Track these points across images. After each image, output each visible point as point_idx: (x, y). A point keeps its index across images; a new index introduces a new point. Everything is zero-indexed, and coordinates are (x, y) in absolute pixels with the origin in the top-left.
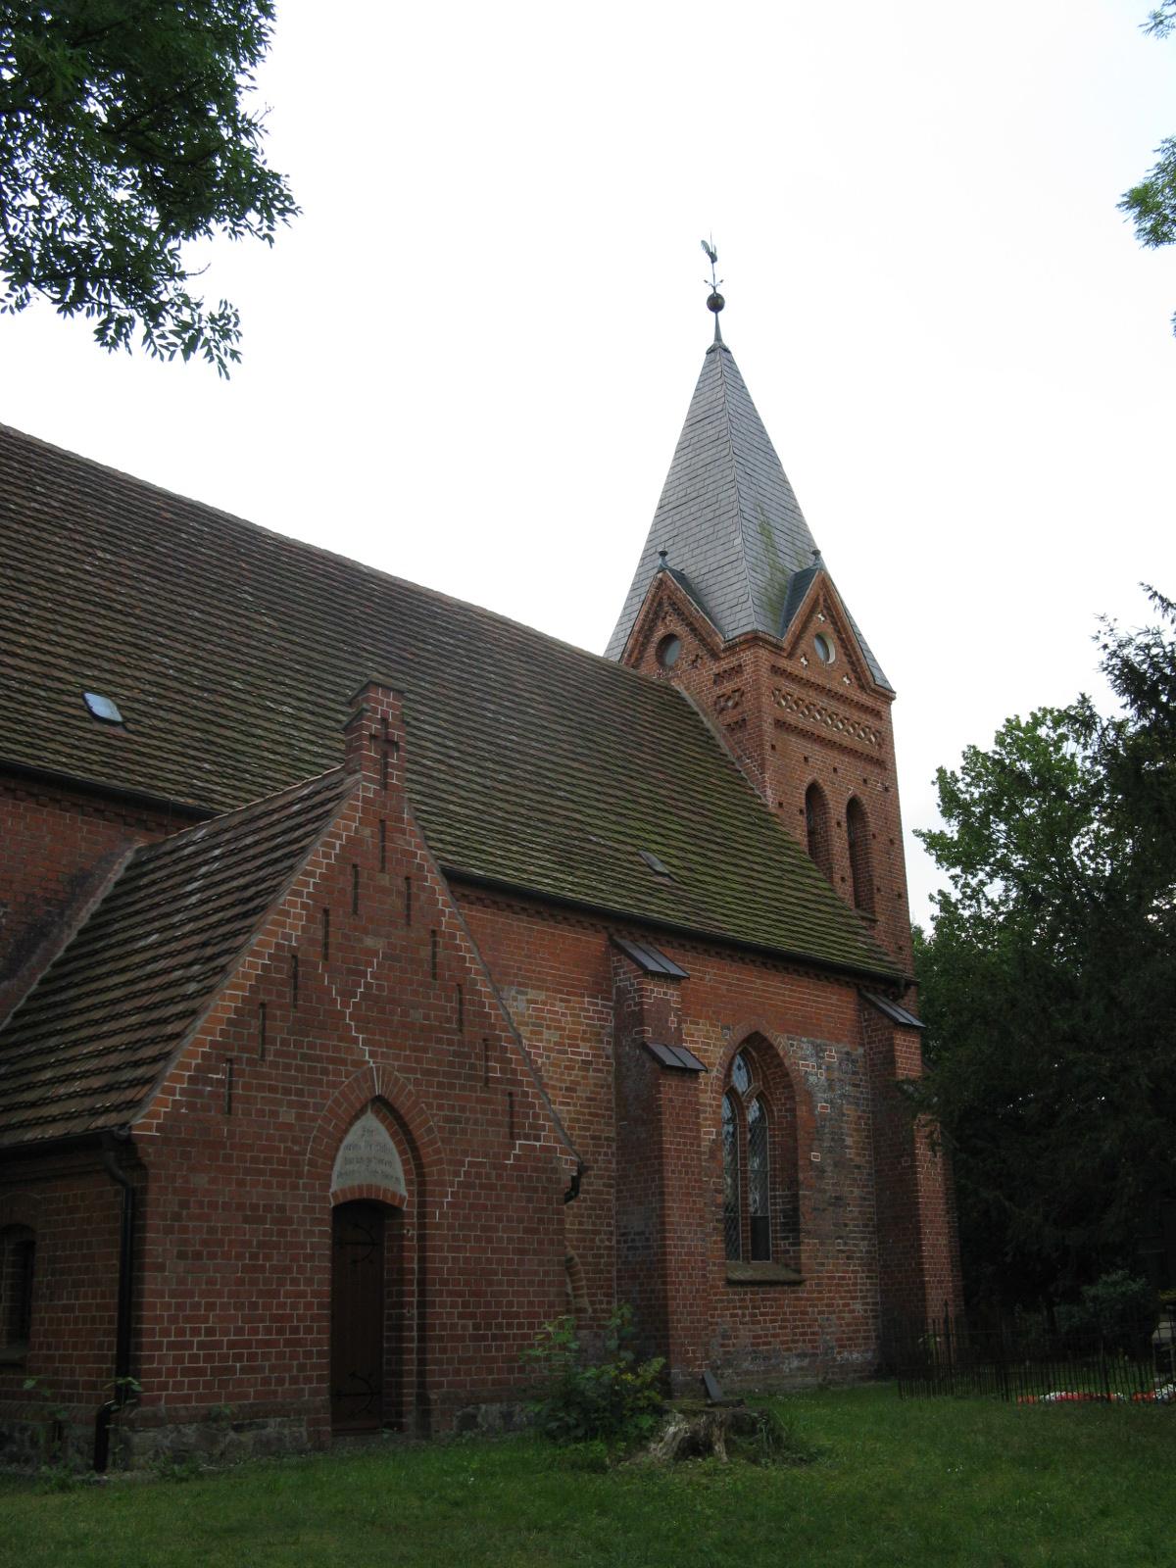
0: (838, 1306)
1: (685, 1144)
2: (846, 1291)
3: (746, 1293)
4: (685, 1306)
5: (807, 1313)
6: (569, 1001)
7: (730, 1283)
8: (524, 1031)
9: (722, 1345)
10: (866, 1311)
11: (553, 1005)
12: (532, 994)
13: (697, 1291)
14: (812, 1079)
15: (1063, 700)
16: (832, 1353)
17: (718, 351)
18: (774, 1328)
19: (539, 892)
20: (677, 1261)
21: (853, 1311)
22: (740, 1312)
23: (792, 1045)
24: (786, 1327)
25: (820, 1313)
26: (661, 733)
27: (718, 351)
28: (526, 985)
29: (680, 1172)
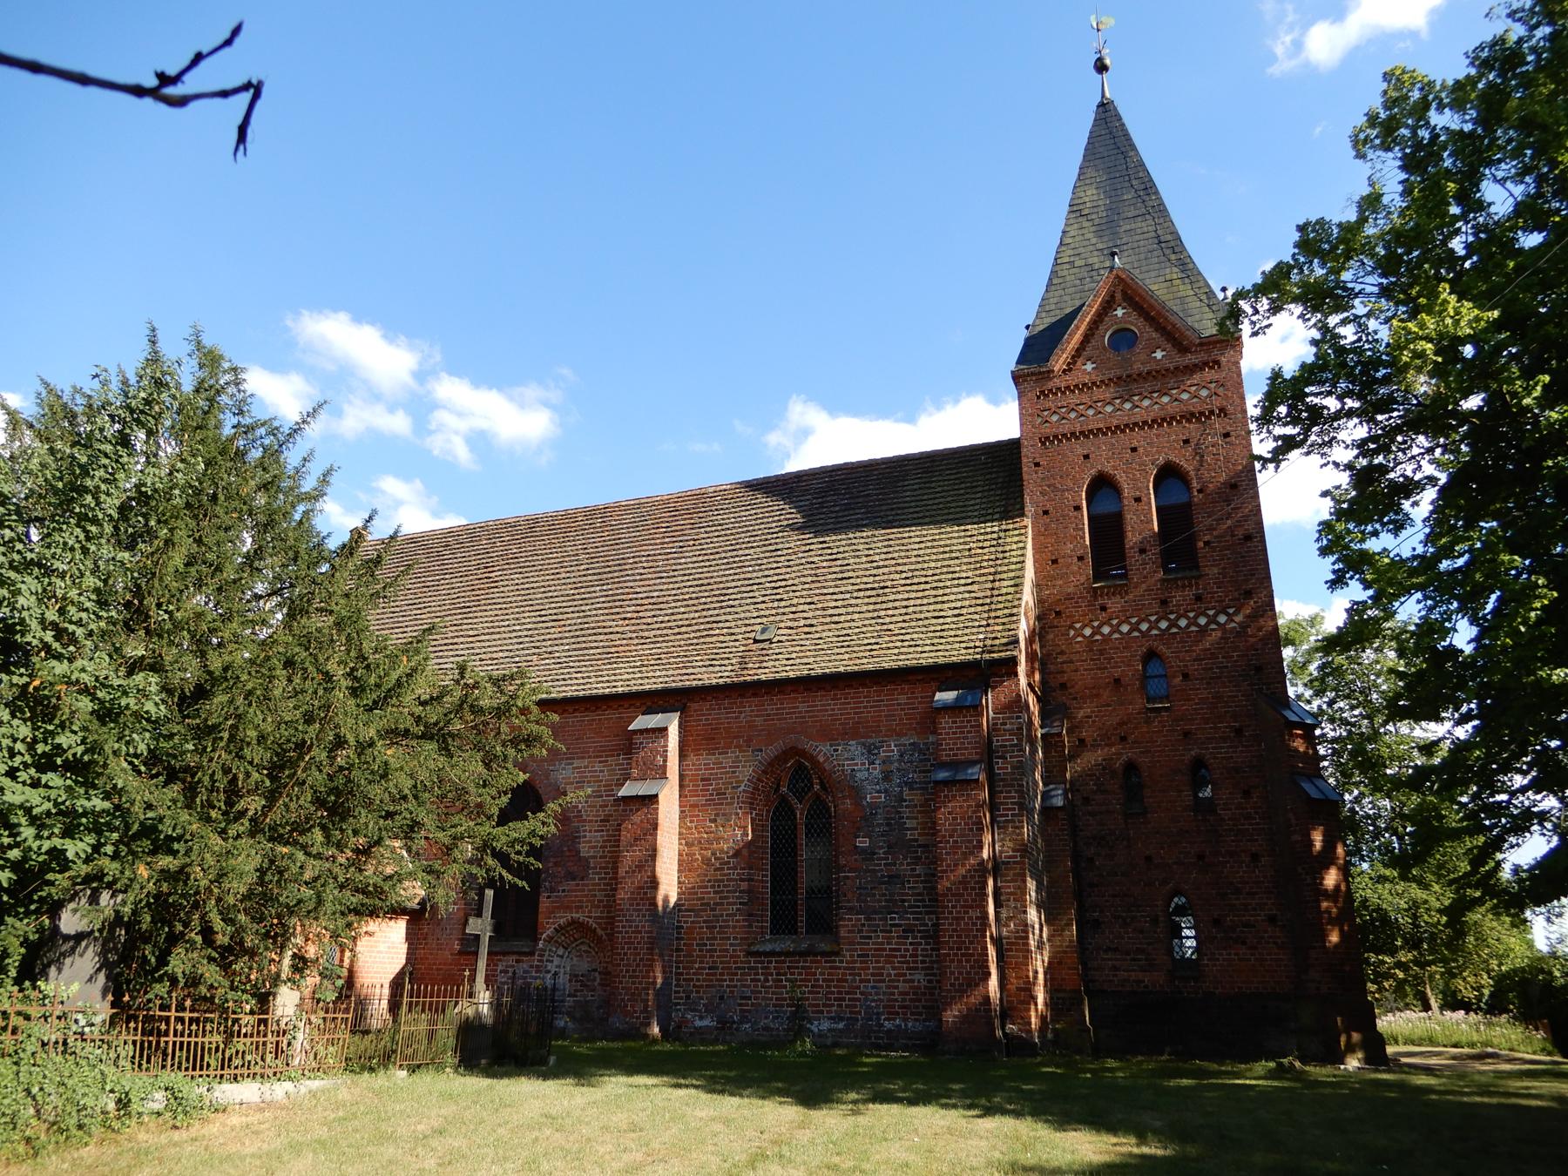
0: (890, 975)
4: (627, 971)
10: (930, 981)
12: (576, 763)
13: (641, 960)
16: (880, 1019)
17: (1106, 110)
20: (623, 938)
23: (836, 750)
27: (1106, 110)
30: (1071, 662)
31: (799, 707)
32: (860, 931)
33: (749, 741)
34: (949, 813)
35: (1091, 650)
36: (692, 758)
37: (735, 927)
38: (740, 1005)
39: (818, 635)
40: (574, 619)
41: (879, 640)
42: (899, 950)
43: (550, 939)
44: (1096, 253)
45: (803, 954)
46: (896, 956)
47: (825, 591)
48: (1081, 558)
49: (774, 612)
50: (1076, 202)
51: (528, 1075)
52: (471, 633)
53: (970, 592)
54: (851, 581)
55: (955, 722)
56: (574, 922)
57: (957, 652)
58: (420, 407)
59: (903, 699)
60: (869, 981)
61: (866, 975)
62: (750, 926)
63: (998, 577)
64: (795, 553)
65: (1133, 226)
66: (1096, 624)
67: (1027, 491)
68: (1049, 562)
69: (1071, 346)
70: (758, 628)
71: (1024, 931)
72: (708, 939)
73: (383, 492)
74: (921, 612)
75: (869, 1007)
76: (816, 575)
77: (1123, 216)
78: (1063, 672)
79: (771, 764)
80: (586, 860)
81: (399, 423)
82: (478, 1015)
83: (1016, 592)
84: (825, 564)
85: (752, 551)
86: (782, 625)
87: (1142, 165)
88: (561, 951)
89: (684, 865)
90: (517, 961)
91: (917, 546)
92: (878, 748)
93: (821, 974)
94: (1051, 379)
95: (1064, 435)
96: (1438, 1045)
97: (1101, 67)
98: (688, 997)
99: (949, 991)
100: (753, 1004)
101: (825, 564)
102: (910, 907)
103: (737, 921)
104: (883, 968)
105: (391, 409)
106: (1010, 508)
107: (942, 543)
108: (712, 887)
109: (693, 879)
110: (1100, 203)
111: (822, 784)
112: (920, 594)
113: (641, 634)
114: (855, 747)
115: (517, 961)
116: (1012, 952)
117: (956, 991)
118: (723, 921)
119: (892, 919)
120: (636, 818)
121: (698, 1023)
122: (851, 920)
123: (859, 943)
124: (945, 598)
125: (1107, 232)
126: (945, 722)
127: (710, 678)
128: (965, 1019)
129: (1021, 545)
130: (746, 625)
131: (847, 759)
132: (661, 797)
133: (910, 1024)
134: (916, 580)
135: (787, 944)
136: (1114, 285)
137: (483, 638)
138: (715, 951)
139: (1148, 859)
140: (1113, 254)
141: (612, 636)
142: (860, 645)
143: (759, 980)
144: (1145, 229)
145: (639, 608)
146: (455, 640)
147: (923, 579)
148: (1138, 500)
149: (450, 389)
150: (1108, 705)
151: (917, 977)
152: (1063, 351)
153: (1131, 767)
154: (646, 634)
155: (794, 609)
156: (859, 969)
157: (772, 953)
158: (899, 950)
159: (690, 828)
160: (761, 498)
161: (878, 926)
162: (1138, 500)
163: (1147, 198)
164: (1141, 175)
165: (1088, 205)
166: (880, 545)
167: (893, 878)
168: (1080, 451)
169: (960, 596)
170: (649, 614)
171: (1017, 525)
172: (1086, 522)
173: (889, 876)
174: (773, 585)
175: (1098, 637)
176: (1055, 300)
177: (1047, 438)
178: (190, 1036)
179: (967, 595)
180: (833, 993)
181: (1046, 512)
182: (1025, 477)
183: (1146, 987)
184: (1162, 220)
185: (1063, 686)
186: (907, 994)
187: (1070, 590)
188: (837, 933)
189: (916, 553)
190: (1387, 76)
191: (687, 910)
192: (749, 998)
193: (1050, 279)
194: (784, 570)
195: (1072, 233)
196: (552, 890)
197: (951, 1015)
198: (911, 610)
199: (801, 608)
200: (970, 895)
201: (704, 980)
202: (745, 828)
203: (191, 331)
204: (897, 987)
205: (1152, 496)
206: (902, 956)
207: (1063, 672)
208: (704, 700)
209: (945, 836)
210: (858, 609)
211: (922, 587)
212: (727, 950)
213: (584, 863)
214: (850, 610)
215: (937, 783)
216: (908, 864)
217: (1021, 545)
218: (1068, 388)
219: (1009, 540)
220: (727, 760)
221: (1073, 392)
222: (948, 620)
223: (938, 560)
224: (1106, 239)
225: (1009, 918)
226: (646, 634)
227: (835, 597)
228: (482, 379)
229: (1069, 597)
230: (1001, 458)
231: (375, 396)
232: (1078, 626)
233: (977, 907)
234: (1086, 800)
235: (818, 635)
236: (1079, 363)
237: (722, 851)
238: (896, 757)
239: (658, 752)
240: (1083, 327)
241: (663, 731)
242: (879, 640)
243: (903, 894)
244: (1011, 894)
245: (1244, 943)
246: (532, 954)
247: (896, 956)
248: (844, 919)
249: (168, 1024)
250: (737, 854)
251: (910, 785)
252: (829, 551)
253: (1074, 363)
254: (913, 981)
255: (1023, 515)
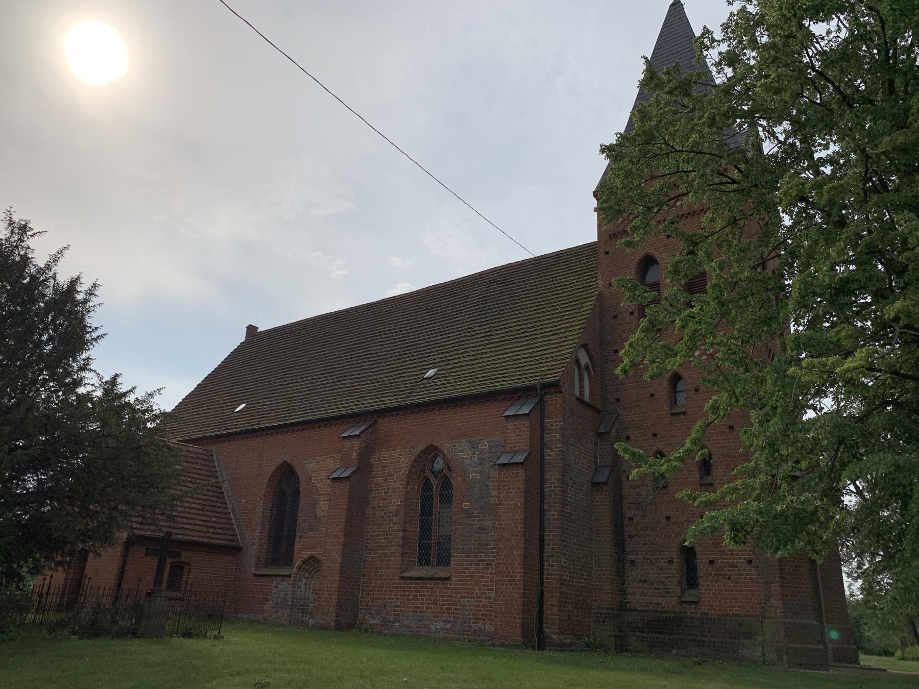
1: (339, 512)
2: (483, 585)
3: (411, 584)
4: (327, 587)
5: (452, 597)
6: (333, 457)
7: (402, 578)
9: (394, 610)
11: (326, 461)
12: (318, 458)
21: (489, 598)
22: (407, 594)
24: (437, 604)
25: (461, 597)
26: (556, 280)
28: (316, 456)
29: (334, 525)
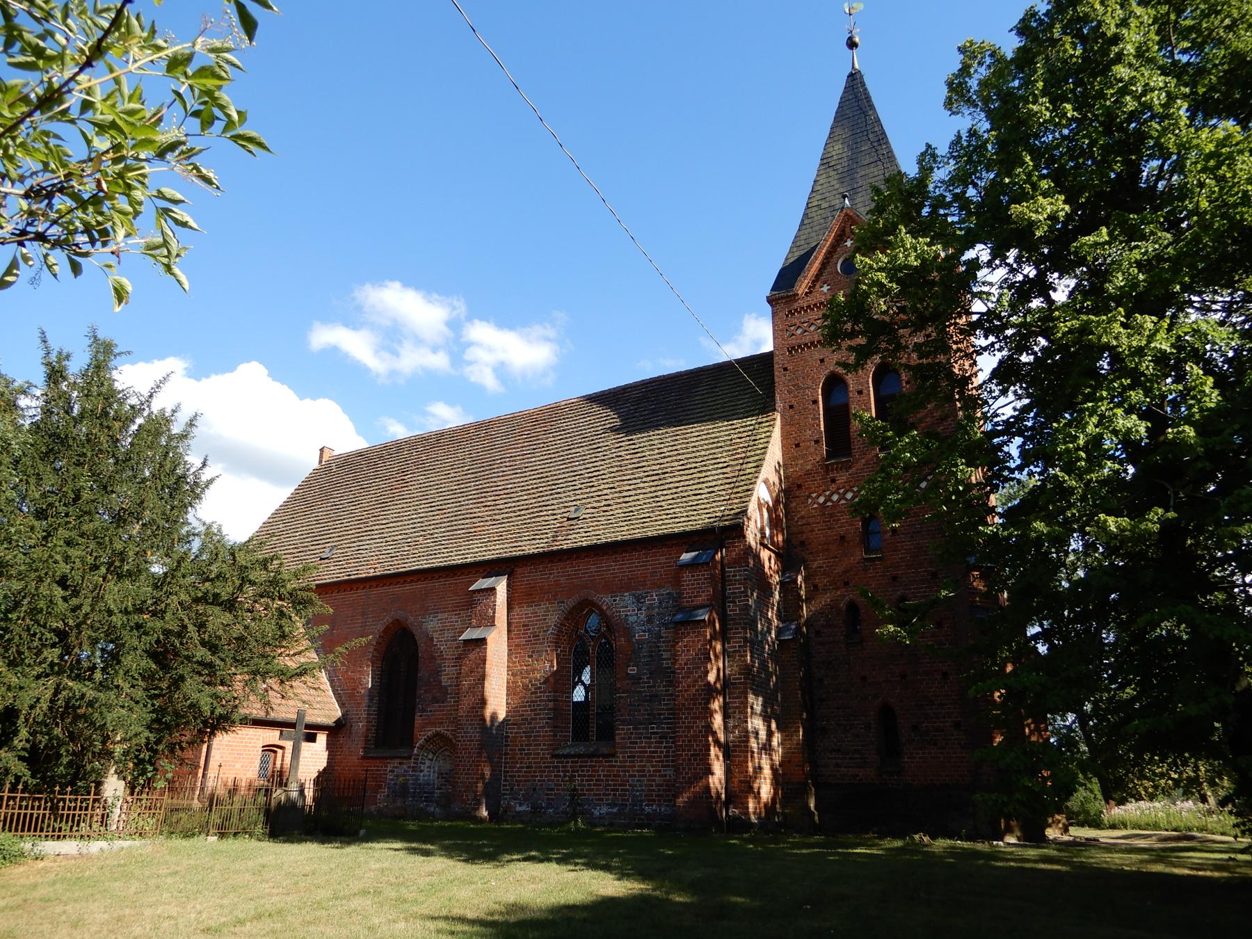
0: (649, 771)
3: (567, 762)
8: (435, 635)
12: (440, 616)
14: (631, 619)
15: (258, 753)
16: (641, 805)
17: (855, 79)
18: (589, 785)
19: (440, 567)
23: (615, 600)
27: (855, 79)
30: (809, 524)
31: (591, 568)
32: (629, 738)
33: (555, 596)
34: (685, 646)
35: (824, 514)
36: (517, 610)
37: (544, 736)
38: (547, 795)
39: (611, 513)
40: (452, 508)
41: (651, 515)
42: (656, 752)
43: (422, 747)
44: (837, 196)
45: (591, 756)
46: (654, 757)
47: (624, 478)
48: (817, 442)
49: (585, 496)
50: (826, 156)
51: (311, 841)
52: (384, 522)
53: (724, 473)
54: (644, 469)
55: (693, 576)
56: (437, 734)
57: (699, 521)
58: (457, 346)
59: (663, 559)
60: (635, 776)
61: (633, 771)
62: (555, 735)
63: (746, 460)
64: (610, 449)
65: (867, 171)
66: (828, 493)
67: (777, 391)
68: (792, 445)
69: (811, 273)
70: (573, 509)
71: (745, 736)
72: (526, 745)
73: (434, 416)
74: (686, 491)
75: (634, 796)
76: (621, 466)
77: (860, 164)
78: (803, 533)
79: (570, 612)
80: (446, 687)
81: (439, 361)
82: (288, 799)
83: (756, 472)
84: (628, 457)
85: (581, 450)
86: (589, 506)
87: (878, 120)
88: (430, 756)
89: (511, 691)
90: (400, 764)
91: (695, 439)
92: (644, 598)
93: (603, 771)
94: (796, 301)
95: (806, 345)
96: (1161, 829)
97: (852, 44)
98: (512, 789)
99: (681, 783)
100: (555, 795)
101: (628, 457)
102: (665, 719)
103: (546, 732)
104: (645, 766)
105: (435, 349)
106: (765, 406)
107: (713, 435)
108: (530, 706)
109: (516, 701)
110: (844, 155)
111: (608, 627)
112: (689, 477)
113: (495, 517)
114: (628, 598)
115: (400, 764)
116: (735, 752)
117: (686, 783)
118: (537, 732)
119: (652, 728)
120: (472, 656)
121: (518, 809)
122: (623, 729)
123: (629, 748)
124: (706, 479)
125: (847, 179)
126: (687, 576)
127: (529, 549)
128: (692, 803)
129: (768, 434)
130: (565, 507)
131: (622, 607)
132: (489, 641)
133: (663, 809)
134: (689, 466)
135: (581, 749)
136: (844, 221)
137: (391, 525)
138: (531, 754)
139: (864, 678)
140: (844, 197)
141: (474, 520)
142: (637, 519)
143: (560, 776)
144: (876, 173)
145: (497, 498)
146: (373, 528)
147: (694, 465)
148: (860, 392)
149: (481, 332)
150: (836, 557)
151: (668, 773)
152: (805, 278)
153: (853, 607)
154: (497, 517)
155: (600, 493)
156: (629, 767)
157: (568, 756)
158: (656, 752)
159: (515, 663)
160: (596, 408)
161: (642, 734)
162: (860, 392)
163: (879, 148)
164: (876, 129)
165: (835, 158)
166: (669, 440)
167: (653, 697)
168: (818, 356)
169: (716, 477)
170: (502, 502)
171: (769, 418)
172: (821, 412)
173: (651, 696)
174: (590, 475)
175: (829, 504)
176: (804, 237)
177: (793, 348)
178: (81, 810)
179: (721, 476)
180: (610, 785)
181: (791, 407)
182: (776, 379)
183: (861, 780)
184: (889, 165)
185: (802, 543)
186: (661, 785)
187: (808, 467)
188: (614, 739)
189: (693, 444)
190: (962, 50)
191: (513, 724)
192: (553, 790)
193: (802, 220)
194: (600, 463)
195: (821, 182)
196: (423, 710)
197: (682, 800)
198: (680, 489)
199: (605, 492)
200: (697, 709)
201: (523, 776)
202: (552, 661)
203: (89, 330)
204: (654, 781)
205: (871, 389)
206: (658, 757)
207: (803, 533)
208: (525, 565)
209: (681, 664)
210: (644, 491)
211: (692, 471)
212: (539, 754)
213: (444, 690)
214: (639, 491)
215: (676, 623)
216: (664, 686)
217: (768, 434)
218: (809, 307)
219: (761, 430)
220: (540, 610)
221: (813, 309)
222: (703, 496)
223: (707, 449)
224: (846, 184)
225: (735, 727)
226: (497, 517)
227: (630, 482)
228: (505, 322)
229: (808, 473)
230: (760, 365)
231: (419, 341)
232: (814, 495)
233: (703, 718)
234: (818, 633)
235: (611, 513)
236: (817, 286)
237: (536, 679)
238: (657, 604)
239: (489, 606)
240: (820, 258)
241: (492, 590)
242: (651, 515)
243: (659, 709)
244: (737, 707)
245: (935, 744)
246: (410, 758)
247: (654, 757)
248: (619, 729)
249: (65, 803)
250: (546, 681)
251: (666, 625)
252: (633, 447)
253: (814, 286)
254: (665, 776)
255: (775, 410)
